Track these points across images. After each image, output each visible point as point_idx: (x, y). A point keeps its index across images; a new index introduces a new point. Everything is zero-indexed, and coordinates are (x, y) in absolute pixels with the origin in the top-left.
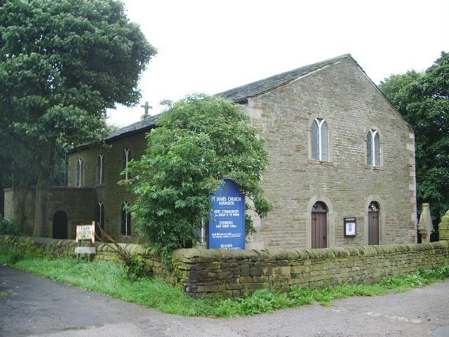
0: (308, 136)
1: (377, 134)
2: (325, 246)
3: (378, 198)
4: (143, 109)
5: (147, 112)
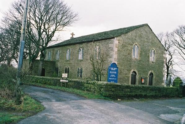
0: (38, 76)
1: (154, 51)
2: (152, 85)
3: (153, 72)
4: (71, 35)
5: (73, 36)
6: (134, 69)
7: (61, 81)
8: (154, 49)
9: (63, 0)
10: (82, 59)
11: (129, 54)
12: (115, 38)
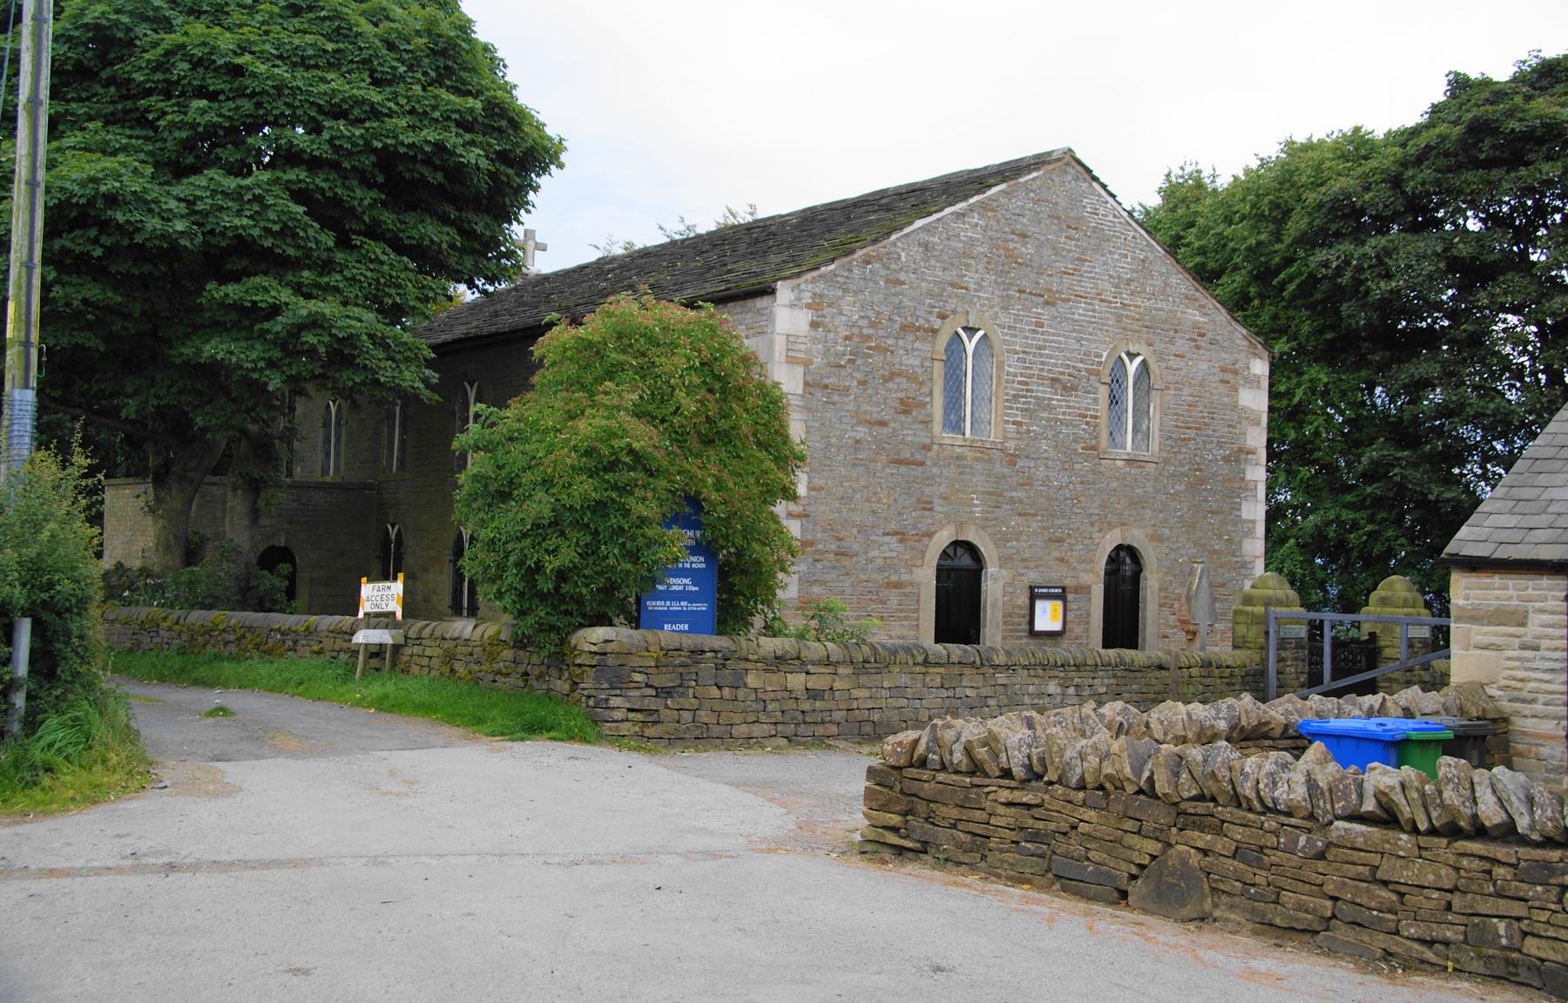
6: (961, 526)
7: (361, 637)
8: (1145, 352)
9: (541, 192)
10: (1056, 626)
11: (906, 407)
12: (784, 291)
